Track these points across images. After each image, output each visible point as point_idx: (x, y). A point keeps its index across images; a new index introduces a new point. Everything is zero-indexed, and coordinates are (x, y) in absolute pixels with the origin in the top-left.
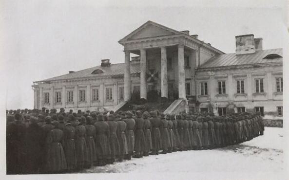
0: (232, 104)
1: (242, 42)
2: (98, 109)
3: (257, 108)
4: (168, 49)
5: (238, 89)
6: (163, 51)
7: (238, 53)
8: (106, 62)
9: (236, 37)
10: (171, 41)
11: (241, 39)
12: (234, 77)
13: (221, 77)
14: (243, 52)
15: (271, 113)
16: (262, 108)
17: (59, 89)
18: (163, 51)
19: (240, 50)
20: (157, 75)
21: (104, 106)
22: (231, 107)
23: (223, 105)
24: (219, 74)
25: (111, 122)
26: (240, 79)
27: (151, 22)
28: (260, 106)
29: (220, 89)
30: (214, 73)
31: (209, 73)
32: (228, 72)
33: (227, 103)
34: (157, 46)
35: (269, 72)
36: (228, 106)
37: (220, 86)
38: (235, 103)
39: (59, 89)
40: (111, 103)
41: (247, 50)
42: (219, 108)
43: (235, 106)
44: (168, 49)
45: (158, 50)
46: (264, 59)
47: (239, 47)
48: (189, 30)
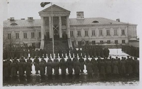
0: (84, 40)
1: (79, 14)
2: (19, 43)
3: (93, 41)
4: (62, 17)
5: (86, 34)
6: (60, 18)
7: (78, 19)
8: (13, 19)
9: (77, 12)
10: (64, 14)
11: (79, 13)
12: (84, 29)
13: (79, 29)
14: (80, 18)
15: (98, 43)
16: (95, 41)
17: (64, 30)
18: (60, 18)
19: (79, 17)
20: (58, 28)
21: (23, 41)
22: (83, 41)
23: (80, 40)
24: (78, 28)
25: (71, 39)
26: (86, 30)
27: (55, 5)
28: (94, 40)
29: (78, 34)
30: (76, 28)
31: (74, 27)
32: (81, 27)
33: (82, 40)
34: (57, 16)
35: (105, 28)
36: (82, 41)
37: (78, 33)
38: (85, 40)
39: (64, 30)
40: (27, 40)
41: (81, 18)
42: (78, 42)
43: (85, 41)
44: (62, 17)
45: (58, 17)
46: (92, 22)
47: (78, 16)
48: (76, 12)
